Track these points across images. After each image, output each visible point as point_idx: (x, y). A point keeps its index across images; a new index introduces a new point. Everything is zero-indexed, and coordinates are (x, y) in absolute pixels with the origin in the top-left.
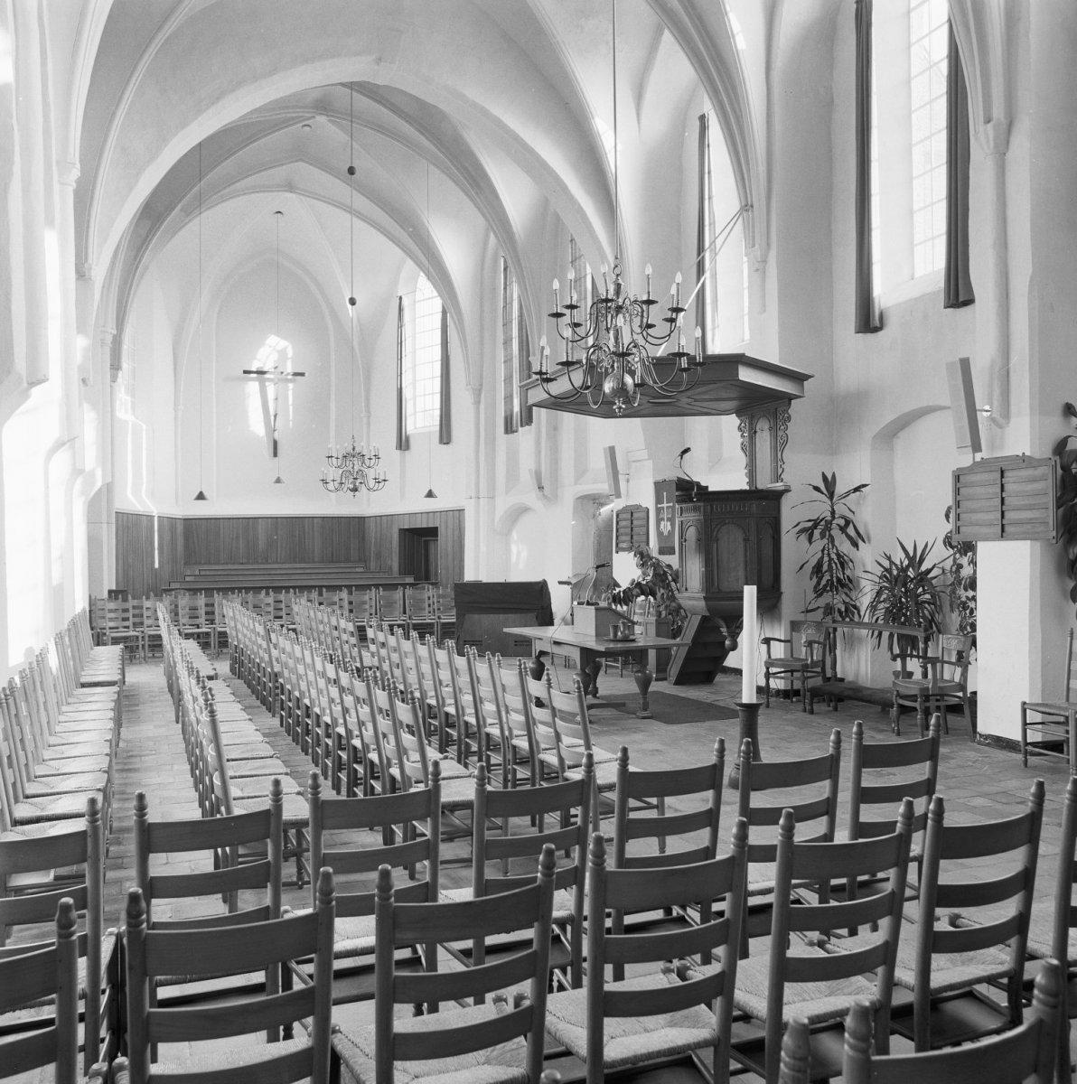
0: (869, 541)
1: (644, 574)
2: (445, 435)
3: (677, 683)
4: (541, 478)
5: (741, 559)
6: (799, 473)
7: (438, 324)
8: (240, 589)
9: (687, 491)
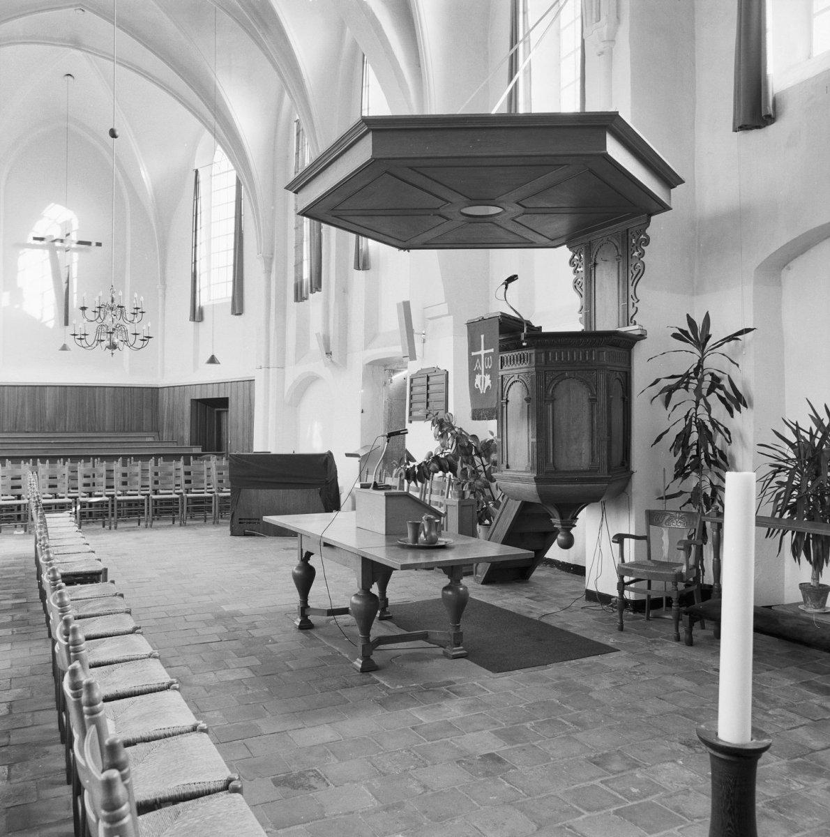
0: (752, 406)
1: (443, 446)
2: (238, 306)
3: (486, 582)
4: (329, 340)
5: (586, 426)
6: (658, 310)
7: (233, 198)
8: (66, 458)
9: (513, 333)
